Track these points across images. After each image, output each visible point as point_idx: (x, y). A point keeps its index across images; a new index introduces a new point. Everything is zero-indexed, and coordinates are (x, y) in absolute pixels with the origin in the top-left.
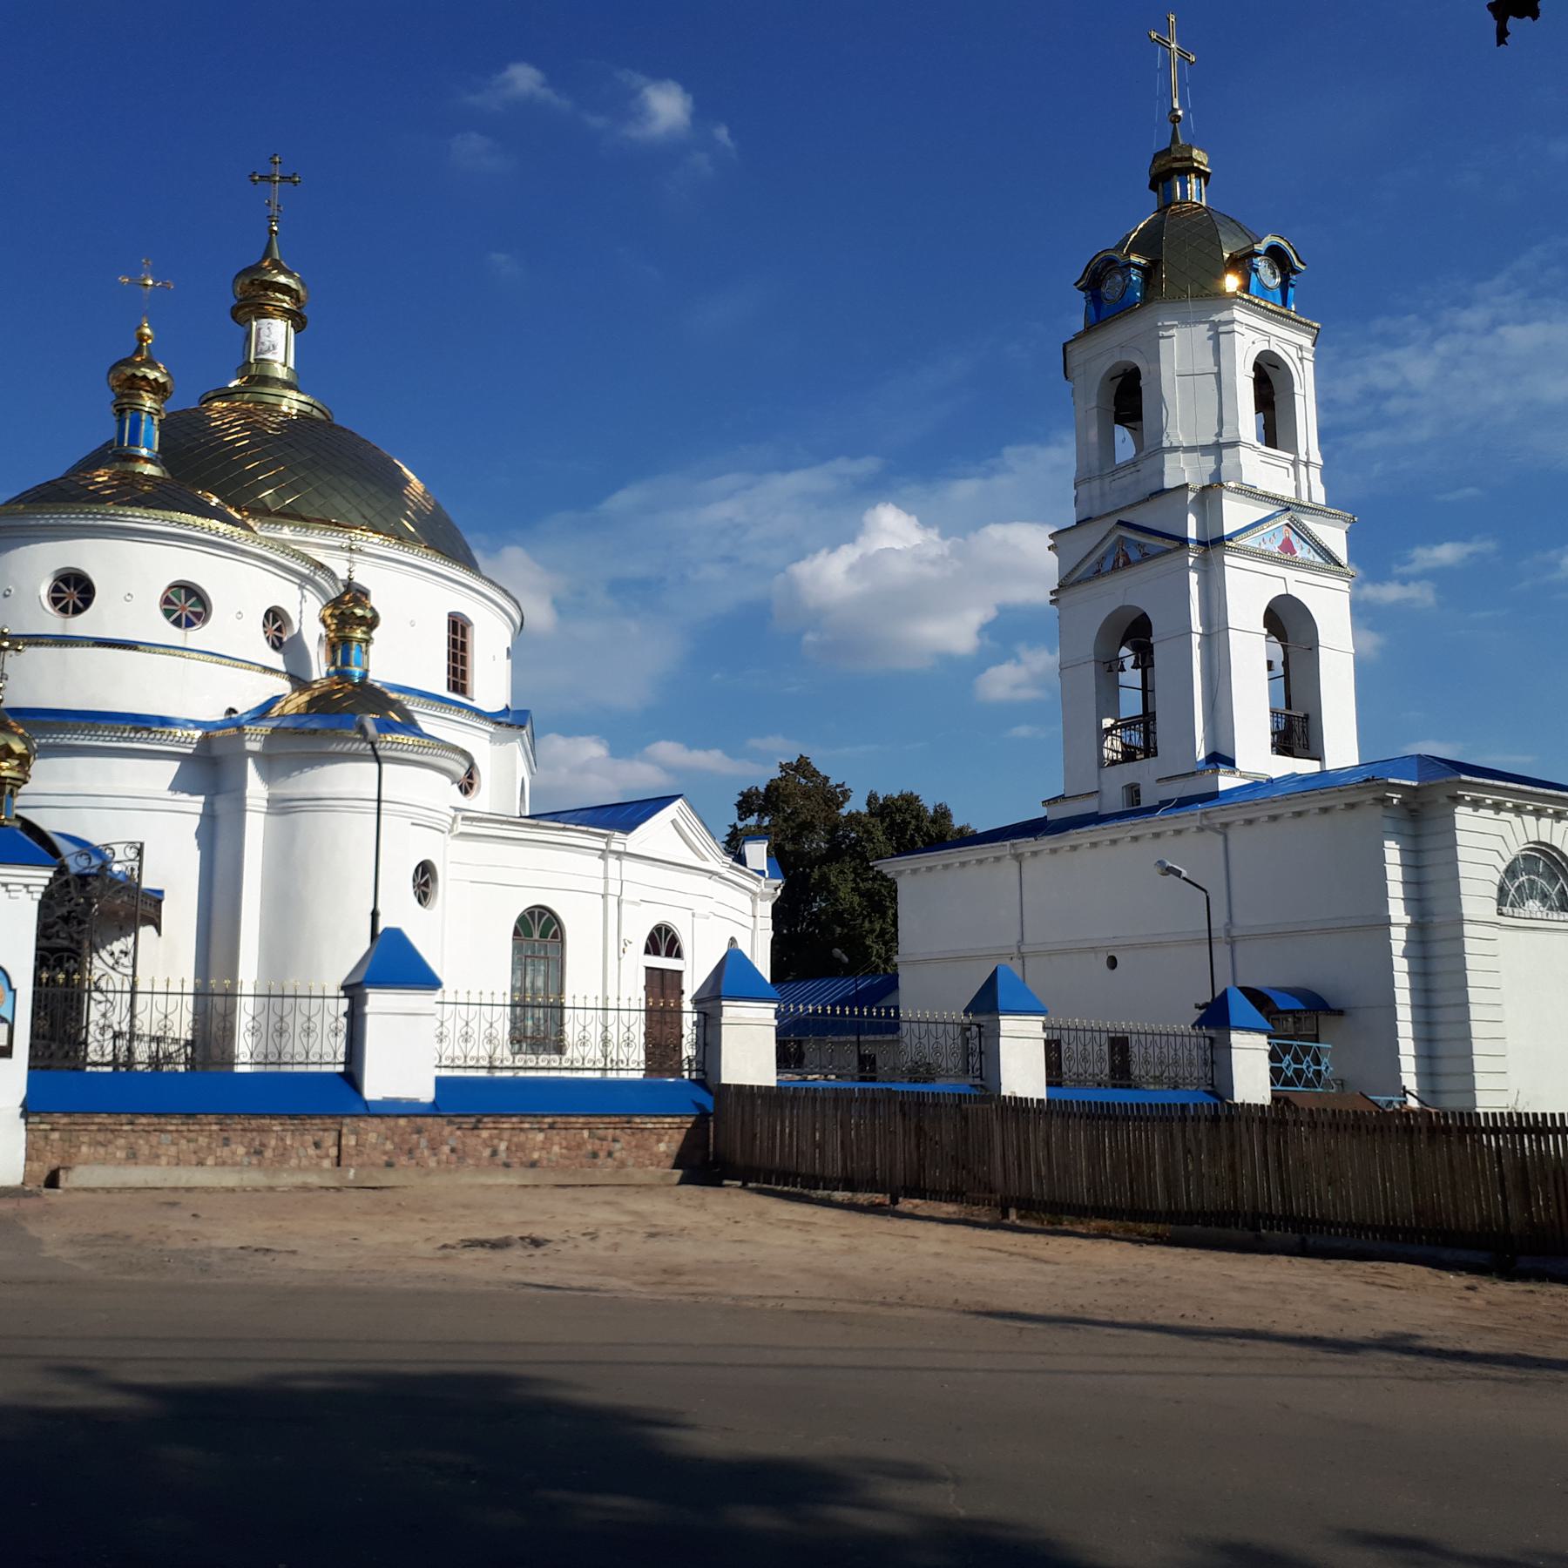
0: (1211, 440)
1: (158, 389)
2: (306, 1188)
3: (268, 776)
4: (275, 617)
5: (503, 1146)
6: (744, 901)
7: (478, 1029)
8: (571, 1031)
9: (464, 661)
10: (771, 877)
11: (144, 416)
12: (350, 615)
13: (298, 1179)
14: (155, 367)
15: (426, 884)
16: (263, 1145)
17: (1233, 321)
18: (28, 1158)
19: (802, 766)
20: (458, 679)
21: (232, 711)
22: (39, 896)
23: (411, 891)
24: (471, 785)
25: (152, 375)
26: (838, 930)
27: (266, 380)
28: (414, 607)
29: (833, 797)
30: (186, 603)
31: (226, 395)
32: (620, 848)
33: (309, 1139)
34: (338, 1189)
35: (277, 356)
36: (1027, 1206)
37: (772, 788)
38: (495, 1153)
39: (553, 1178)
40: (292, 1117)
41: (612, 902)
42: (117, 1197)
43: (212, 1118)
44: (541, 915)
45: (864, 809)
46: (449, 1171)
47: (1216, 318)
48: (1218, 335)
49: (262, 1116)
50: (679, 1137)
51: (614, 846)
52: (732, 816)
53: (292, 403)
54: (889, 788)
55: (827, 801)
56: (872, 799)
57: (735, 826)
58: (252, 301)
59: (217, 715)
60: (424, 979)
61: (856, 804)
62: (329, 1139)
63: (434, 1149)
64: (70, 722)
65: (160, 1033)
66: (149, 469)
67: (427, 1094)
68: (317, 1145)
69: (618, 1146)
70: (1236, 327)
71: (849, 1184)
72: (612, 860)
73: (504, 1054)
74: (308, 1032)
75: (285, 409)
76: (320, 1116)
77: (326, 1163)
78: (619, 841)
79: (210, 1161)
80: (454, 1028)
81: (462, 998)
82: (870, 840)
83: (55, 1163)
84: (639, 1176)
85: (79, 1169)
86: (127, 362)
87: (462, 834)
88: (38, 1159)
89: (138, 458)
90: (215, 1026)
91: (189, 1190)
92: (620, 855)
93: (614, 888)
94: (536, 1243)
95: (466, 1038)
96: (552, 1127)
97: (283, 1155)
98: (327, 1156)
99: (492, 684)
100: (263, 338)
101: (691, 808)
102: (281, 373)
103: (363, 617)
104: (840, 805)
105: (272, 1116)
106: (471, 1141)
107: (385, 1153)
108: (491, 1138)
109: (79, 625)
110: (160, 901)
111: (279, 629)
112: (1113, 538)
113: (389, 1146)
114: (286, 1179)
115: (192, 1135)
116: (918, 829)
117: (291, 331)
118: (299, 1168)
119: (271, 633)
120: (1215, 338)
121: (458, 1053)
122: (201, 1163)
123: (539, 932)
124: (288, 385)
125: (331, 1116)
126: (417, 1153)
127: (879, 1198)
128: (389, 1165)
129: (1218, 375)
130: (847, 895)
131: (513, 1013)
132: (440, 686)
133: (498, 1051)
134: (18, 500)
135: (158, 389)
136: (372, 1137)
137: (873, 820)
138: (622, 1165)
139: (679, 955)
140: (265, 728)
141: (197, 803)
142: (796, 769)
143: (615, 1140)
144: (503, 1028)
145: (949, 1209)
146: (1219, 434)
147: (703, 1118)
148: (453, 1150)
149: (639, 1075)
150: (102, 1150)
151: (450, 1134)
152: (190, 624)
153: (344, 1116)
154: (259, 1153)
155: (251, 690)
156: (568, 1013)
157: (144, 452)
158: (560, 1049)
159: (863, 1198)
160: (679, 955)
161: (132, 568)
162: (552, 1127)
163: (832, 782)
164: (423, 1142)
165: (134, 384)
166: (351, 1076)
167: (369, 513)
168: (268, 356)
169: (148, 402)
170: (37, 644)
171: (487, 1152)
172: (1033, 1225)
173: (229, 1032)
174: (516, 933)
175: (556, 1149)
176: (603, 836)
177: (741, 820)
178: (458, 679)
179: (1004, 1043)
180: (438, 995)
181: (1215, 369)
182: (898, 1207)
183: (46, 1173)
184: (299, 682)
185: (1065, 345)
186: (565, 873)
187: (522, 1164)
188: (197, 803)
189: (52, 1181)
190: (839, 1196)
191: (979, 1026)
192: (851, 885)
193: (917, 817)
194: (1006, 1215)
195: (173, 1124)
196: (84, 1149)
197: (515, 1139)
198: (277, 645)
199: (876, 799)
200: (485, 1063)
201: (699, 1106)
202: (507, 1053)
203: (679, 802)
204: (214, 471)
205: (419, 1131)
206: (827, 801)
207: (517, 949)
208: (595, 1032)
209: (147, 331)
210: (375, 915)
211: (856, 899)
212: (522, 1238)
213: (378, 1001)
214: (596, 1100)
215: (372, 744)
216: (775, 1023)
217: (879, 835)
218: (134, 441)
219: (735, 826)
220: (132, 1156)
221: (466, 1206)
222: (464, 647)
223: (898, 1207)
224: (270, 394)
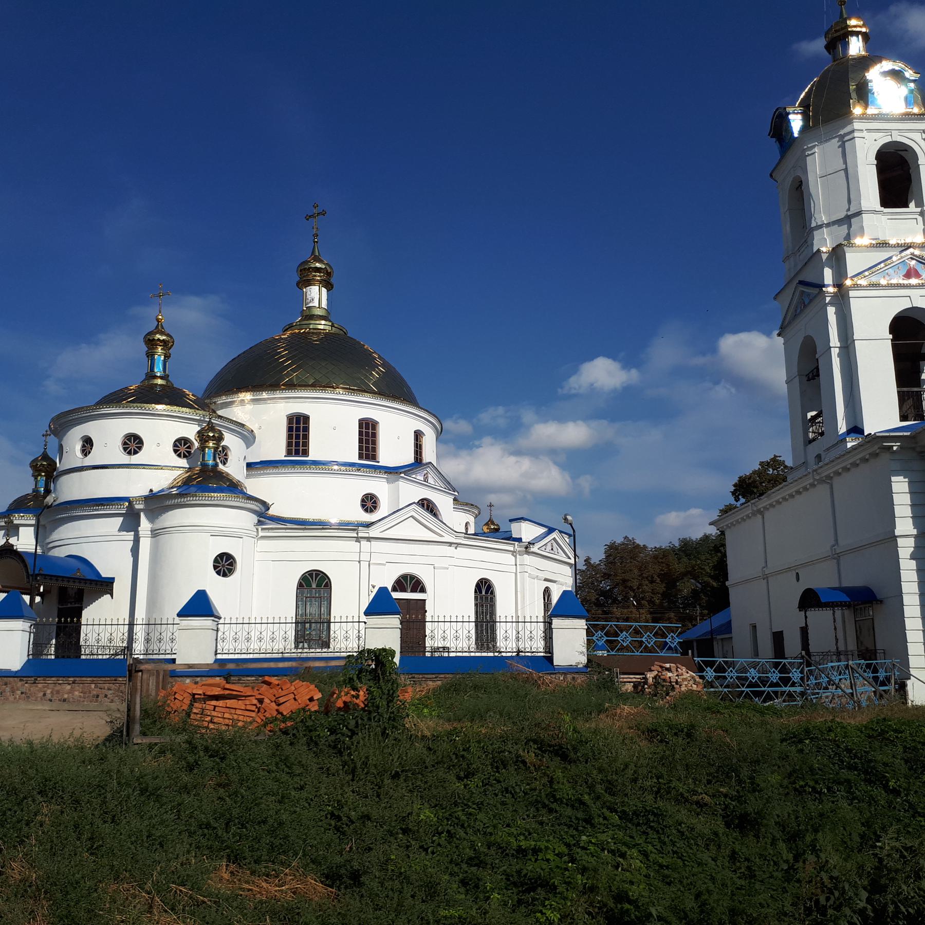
0: (842, 215)
3: (151, 519)
5: (49, 691)
6: (510, 558)
7: (279, 635)
17: (853, 131)
27: (312, 317)
32: (367, 535)
38: (44, 695)
41: (364, 565)
44: (317, 575)
47: (842, 132)
48: (845, 142)
51: (360, 535)
70: (856, 134)
72: (364, 543)
74: (172, 640)
80: (254, 635)
81: (460, 619)
86: (150, 333)
87: (263, 537)
92: (369, 539)
108: (44, 687)
111: (189, 447)
112: (797, 294)
120: (843, 146)
129: (846, 170)
132: (353, 456)
139: (423, 590)
143: (109, 689)
144: (291, 634)
146: (849, 210)
149: (53, 657)
158: (327, 645)
160: (423, 590)
161: (108, 432)
164: (8, 689)
166: (550, 659)
168: (311, 305)
174: (300, 585)
181: (844, 167)
185: (771, 176)
187: (60, 700)
197: (56, 689)
205: (6, 684)
208: (512, 634)
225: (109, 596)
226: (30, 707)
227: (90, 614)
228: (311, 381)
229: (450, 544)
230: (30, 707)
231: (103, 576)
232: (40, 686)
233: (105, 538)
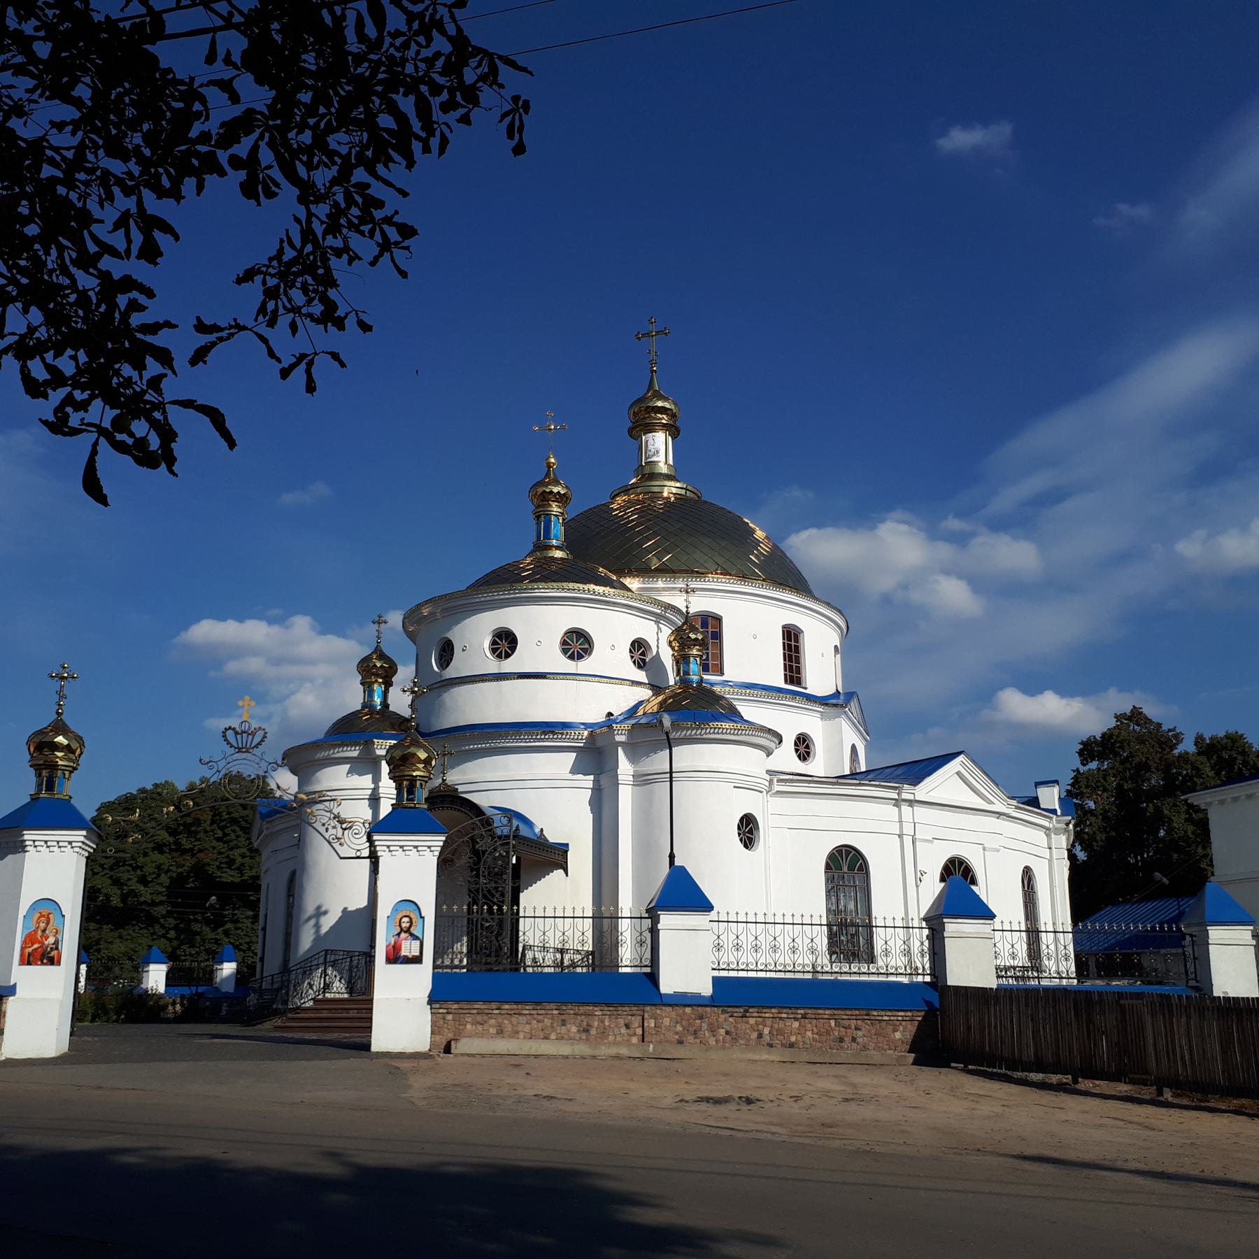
1: (563, 499)
2: (618, 1057)
3: (633, 758)
4: (639, 647)
5: (766, 1031)
6: (1040, 837)
8: (879, 945)
9: (798, 660)
10: (1063, 814)
11: (553, 518)
12: (701, 636)
13: (613, 1051)
14: (557, 483)
15: (751, 832)
16: (588, 1025)
18: (433, 1033)
19: (1136, 715)
20: (793, 671)
21: (610, 714)
22: (437, 853)
23: (738, 839)
24: (808, 754)
25: (555, 490)
26: (1175, 856)
27: (653, 476)
28: (751, 623)
29: (1165, 740)
30: (577, 644)
31: (626, 490)
32: (911, 797)
33: (621, 1021)
34: (641, 1059)
35: (661, 458)
36: (1179, 1086)
37: (1107, 737)
38: (760, 1036)
39: (805, 1057)
40: (608, 1005)
41: (908, 841)
42: (477, 1060)
43: (552, 1006)
44: (848, 853)
45: (1192, 749)
46: (724, 1048)
49: (587, 1004)
50: (912, 1028)
51: (904, 796)
52: (1076, 762)
53: (670, 489)
54: (1215, 729)
55: (1161, 744)
56: (1199, 740)
57: (1078, 770)
58: (641, 425)
59: (601, 718)
60: (701, 904)
61: (1187, 746)
62: (636, 1021)
63: (713, 1031)
64: (503, 731)
65: (560, 946)
66: (558, 554)
67: (707, 990)
68: (627, 1026)
69: (860, 1033)
71: (1040, 1067)
72: (905, 808)
73: (824, 960)
75: (665, 494)
76: (628, 1004)
77: (635, 1040)
78: (908, 792)
79: (553, 1036)
80: (728, 940)
82: (1199, 776)
83: (450, 1036)
84: (876, 1057)
85: (464, 1041)
86: (541, 483)
88: (439, 1033)
89: (550, 547)
90: (607, 940)
91: (536, 1056)
92: (911, 803)
93: (908, 829)
94: (749, 1101)
95: (756, 949)
96: (804, 1017)
97: (603, 1033)
98: (635, 1034)
99: (822, 674)
100: (650, 447)
101: (973, 761)
102: (663, 468)
103: (696, 639)
104: (1173, 747)
105: (594, 1004)
106: (742, 1026)
107: (676, 1033)
109: (509, 666)
110: (566, 852)
111: (643, 654)
113: (679, 1028)
114: (604, 1051)
115: (540, 1017)
116: (1245, 763)
117: (670, 439)
118: (615, 1043)
119: (637, 656)
121: (788, 961)
122: (546, 1038)
123: (847, 868)
124: (669, 477)
125: (636, 1005)
126: (700, 1034)
127: (1067, 1079)
128: (680, 1042)
130: (1179, 821)
131: (830, 930)
132: (778, 680)
133: (819, 961)
134: (473, 585)
135: (563, 499)
136: (667, 1021)
137: (1201, 758)
138: (865, 1048)
140: (627, 725)
141: (589, 781)
142: (1130, 718)
143: (857, 1029)
144: (822, 942)
145: (1123, 1088)
147: (931, 1012)
148: (727, 1033)
150: (480, 1027)
151: (726, 1020)
152: (580, 657)
153: (645, 1005)
154: (586, 1031)
155: (621, 699)
156: (521, 920)
157: (554, 542)
158: (871, 959)
159: (1054, 1078)
161: (540, 624)
162: (804, 1017)
163: (1165, 728)
164: (705, 1026)
165: (546, 498)
166: (653, 978)
167: (720, 560)
169: (555, 508)
170: (483, 681)
171: (754, 1035)
172: (1185, 1102)
173: (616, 945)
174: (828, 867)
175: (809, 1034)
176: (895, 788)
177: (1084, 765)
178: (793, 671)
179: (1213, 950)
180: (713, 915)
182: (1078, 1086)
183: (444, 1042)
184: (656, 689)
186: (869, 822)
188: (589, 781)
189: (447, 1050)
190: (1036, 1077)
191: (1191, 936)
192: (1184, 816)
193: (1244, 753)
194: (1160, 1093)
195: (526, 1010)
196: (469, 1026)
198: (641, 664)
199: (1203, 739)
200: (810, 969)
201: (928, 1003)
202: (826, 961)
203: (961, 758)
204: (602, 550)
205: (701, 1018)
206: (1161, 744)
207: (829, 880)
209: (552, 460)
210: (672, 857)
211: (1191, 828)
212: (740, 1098)
213: (667, 920)
214: (887, 996)
215: (667, 733)
216: (1254, 942)
217: (1208, 770)
218: (547, 536)
219: (1078, 770)
220: (500, 1032)
221: (726, 1075)
222: (797, 649)
223: (1078, 1086)
224: (655, 485)
225: (561, 871)
226: (750, 1056)
227: (534, 898)
228: (655, 564)
229: (999, 814)
230: (750, 1056)
231: (551, 840)
232: (752, 1021)
233: (552, 784)
